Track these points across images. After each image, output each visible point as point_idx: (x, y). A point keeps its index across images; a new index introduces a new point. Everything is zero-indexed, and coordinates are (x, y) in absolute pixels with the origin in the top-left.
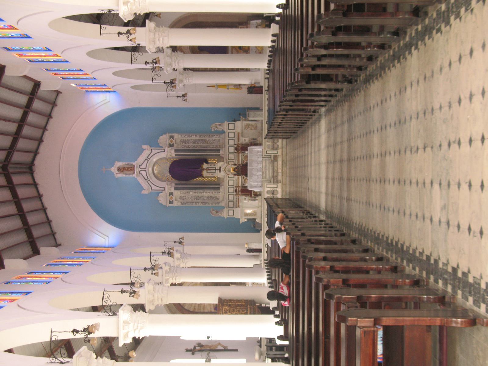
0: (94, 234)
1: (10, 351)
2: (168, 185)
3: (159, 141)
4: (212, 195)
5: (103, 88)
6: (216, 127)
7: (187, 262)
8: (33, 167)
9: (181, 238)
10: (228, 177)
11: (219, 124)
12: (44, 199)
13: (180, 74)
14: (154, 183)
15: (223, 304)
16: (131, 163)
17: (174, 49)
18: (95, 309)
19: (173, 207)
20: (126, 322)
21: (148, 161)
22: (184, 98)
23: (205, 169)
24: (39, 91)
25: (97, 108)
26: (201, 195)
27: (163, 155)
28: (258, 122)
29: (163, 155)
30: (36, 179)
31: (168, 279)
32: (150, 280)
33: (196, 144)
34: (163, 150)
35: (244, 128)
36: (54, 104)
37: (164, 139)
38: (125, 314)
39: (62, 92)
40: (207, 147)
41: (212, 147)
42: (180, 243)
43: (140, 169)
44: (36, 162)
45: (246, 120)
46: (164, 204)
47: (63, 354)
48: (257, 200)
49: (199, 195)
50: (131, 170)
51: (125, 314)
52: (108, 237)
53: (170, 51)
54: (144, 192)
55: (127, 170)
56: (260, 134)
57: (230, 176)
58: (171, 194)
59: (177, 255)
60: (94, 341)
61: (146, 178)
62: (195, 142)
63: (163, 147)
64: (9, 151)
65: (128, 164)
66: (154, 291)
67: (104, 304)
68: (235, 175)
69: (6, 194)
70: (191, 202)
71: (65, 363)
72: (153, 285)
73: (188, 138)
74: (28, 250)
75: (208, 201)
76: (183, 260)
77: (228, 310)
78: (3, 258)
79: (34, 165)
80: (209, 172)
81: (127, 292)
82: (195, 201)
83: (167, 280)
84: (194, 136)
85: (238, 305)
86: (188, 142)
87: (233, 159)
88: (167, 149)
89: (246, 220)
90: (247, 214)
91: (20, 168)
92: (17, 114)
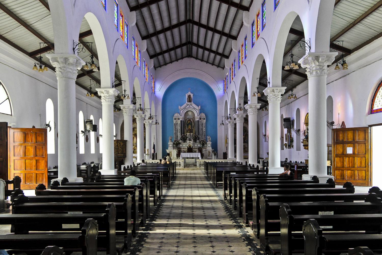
0: (160, 85)
1: (117, 63)
5: (225, 89)
6: (209, 139)
8: (190, 57)
9: (128, 96)
13: (233, 122)
16: (192, 101)
17: (235, 124)
18: (134, 94)
20: (108, 92)
22: (222, 124)
23: (190, 134)
24: (224, 58)
27: (196, 115)
30: (185, 58)
31: (138, 117)
33: (201, 130)
36: (218, 66)
37: (203, 115)
38: (113, 92)
42: (156, 123)
44: (192, 59)
46: (174, 116)
47: (79, 50)
50: (189, 101)
51: (113, 92)
53: (235, 123)
54: (179, 107)
55: (189, 99)
56: (206, 158)
58: (179, 119)
59: (151, 121)
60: (86, 67)
61: (186, 108)
62: (202, 129)
64: (199, 23)
65: (192, 100)
67: (136, 98)
68: (188, 147)
71: (74, 51)
72: (132, 108)
73: (204, 126)
74: (152, 53)
79: (191, 58)
81: (125, 93)
82: (176, 130)
83: (137, 116)
86: (202, 126)
88: (199, 117)
91: (190, 50)
92: (219, 28)
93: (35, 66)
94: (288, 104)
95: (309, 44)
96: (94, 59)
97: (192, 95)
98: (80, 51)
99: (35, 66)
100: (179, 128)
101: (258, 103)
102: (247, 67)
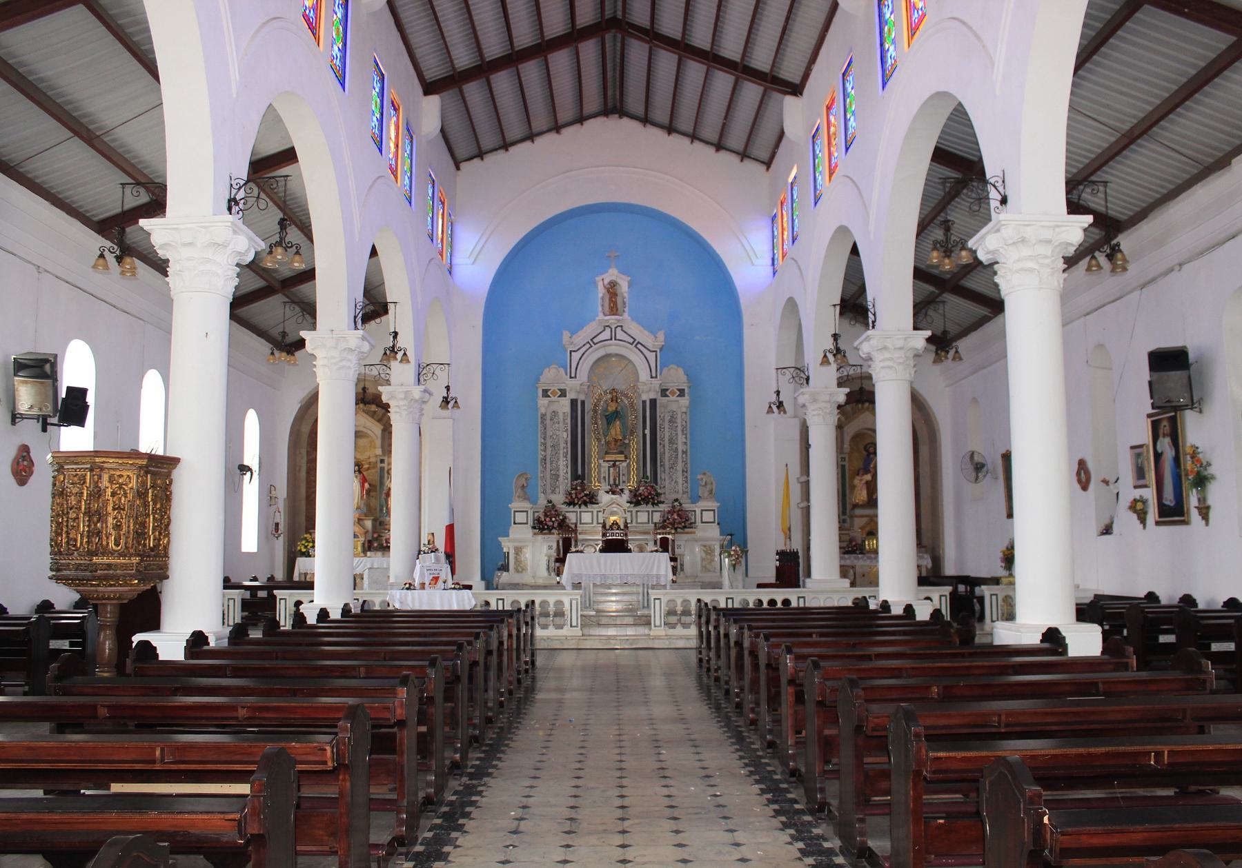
0: (480, 235)
1: (374, 252)
2: (581, 385)
3: (675, 366)
4: (561, 479)
7: (401, 416)
8: (617, 116)
9: (456, 402)
10: (598, 512)
11: (712, 490)
12: (551, 137)
14: (585, 355)
15: (147, 473)
16: (626, 309)
19: (537, 397)
21: (632, 344)
25: (738, 238)
26: (561, 455)
27: (644, 375)
28: (719, 574)
29: (644, 375)
32: (431, 394)
33: (667, 447)
34: (654, 375)
35: (704, 543)
39: (770, 170)
40: (661, 466)
41: (663, 477)
42: (446, 401)
43: (613, 327)
44: (626, 120)
45: (722, 547)
46: (542, 379)
48: (550, 575)
49: (561, 452)
52: (474, 263)
54: (566, 336)
55: (610, 300)
57: (600, 514)
61: (595, 340)
62: (671, 442)
63: (660, 374)
66: (345, 349)
69: (556, 24)
70: (545, 433)
73: (679, 425)
75: (548, 470)
76: (405, 405)
77: (120, 488)
78: (444, 94)
79: (620, 117)
80: (609, 471)
82: (549, 444)
84: (684, 440)
85: (143, 525)
87: (639, 521)
88: (656, 383)
89: (505, 550)
90: (518, 551)
92: (731, 48)
93: (102, 256)
94: (1144, 286)
95: (1001, 189)
96: (293, 235)
97: (624, 287)
98: (249, 204)
99: (102, 256)
100: (565, 436)
101: (915, 328)
102: (970, 24)
